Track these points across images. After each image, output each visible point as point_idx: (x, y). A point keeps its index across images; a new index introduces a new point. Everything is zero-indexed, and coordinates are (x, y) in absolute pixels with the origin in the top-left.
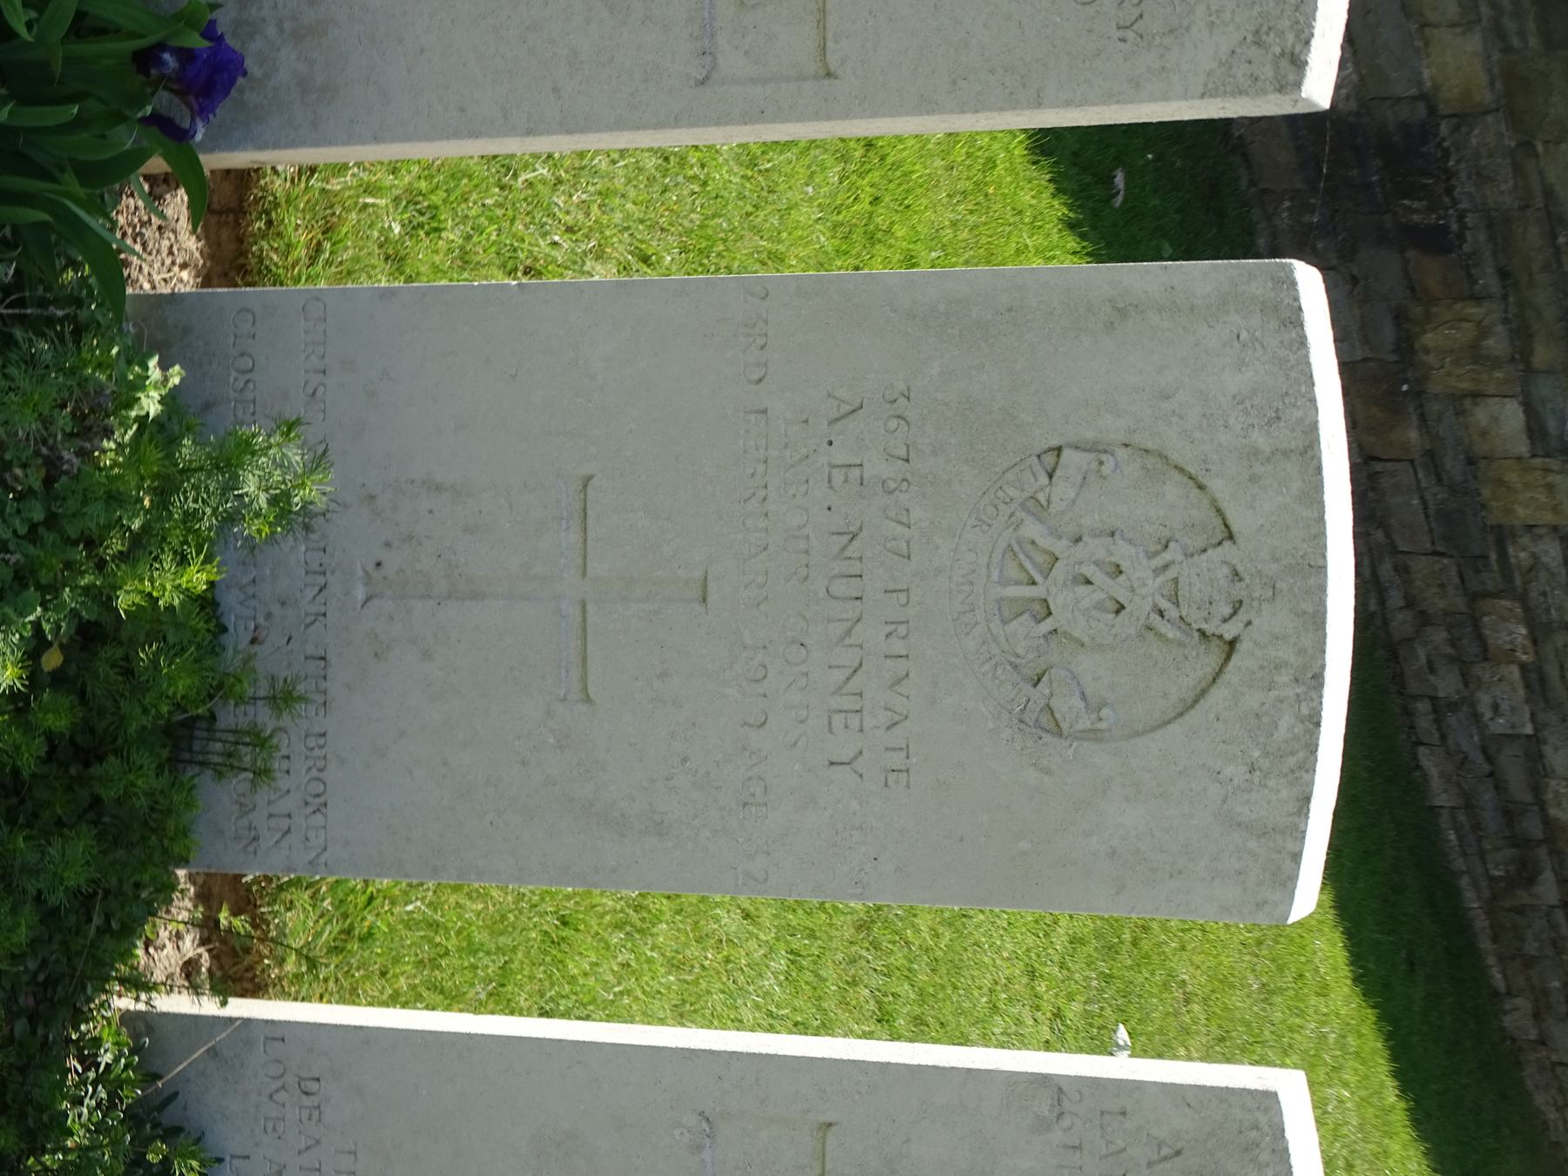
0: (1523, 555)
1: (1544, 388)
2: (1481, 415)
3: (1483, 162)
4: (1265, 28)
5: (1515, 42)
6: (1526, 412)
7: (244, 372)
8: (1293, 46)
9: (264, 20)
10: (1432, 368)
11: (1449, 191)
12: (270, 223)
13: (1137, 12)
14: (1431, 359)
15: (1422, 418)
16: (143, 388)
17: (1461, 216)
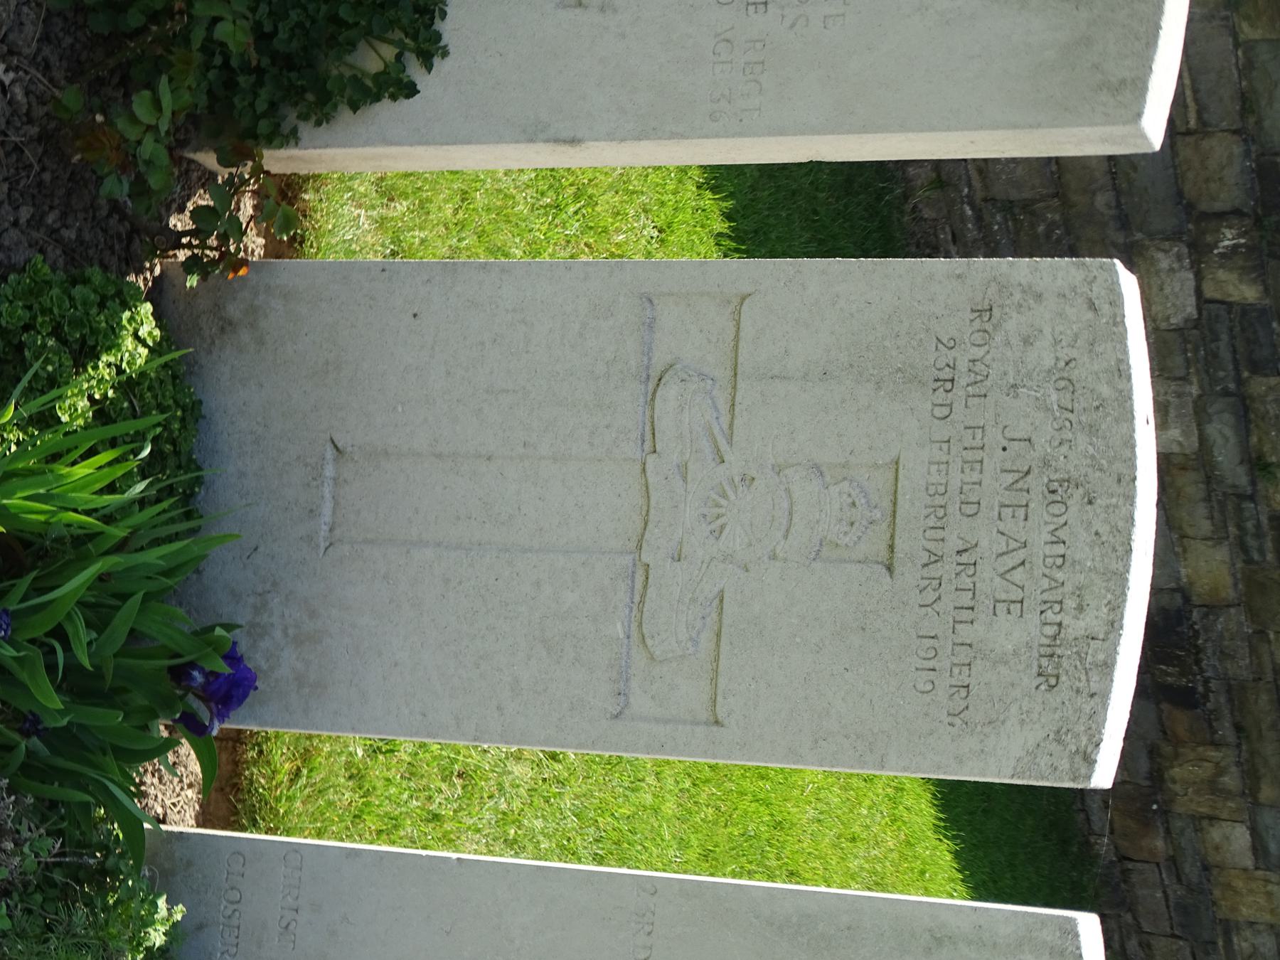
0: (1244, 945)
1: (1267, 818)
2: (1215, 834)
3: (1226, 643)
4: (1064, 730)
5: (1256, 556)
6: (1251, 835)
7: (232, 903)
8: (1086, 747)
9: (272, 625)
10: (1177, 794)
11: (1198, 662)
12: (261, 752)
13: (963, 704)
14: (1177, 788)
15: (1168, 831)
16: (153, 923)
17: (1206, 681)
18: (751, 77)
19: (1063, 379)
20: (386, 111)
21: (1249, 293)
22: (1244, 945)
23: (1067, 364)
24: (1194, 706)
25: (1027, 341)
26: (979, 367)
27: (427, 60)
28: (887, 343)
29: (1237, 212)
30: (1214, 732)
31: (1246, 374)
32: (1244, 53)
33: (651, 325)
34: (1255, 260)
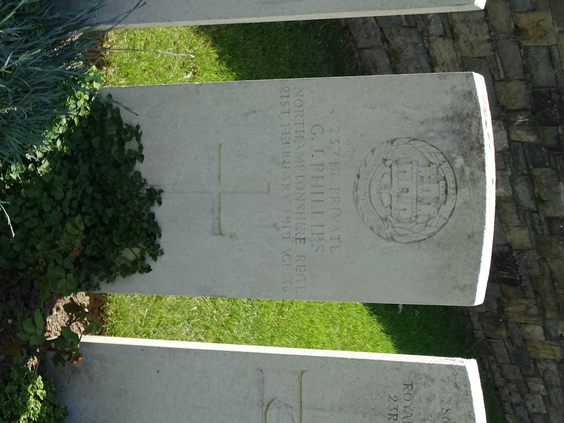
0: (542, 367)
2: (528, 329)
5: (540, 232)
15: (507, 328)
17: (521, 277)
18: (300, 272)
19: (445, 417)
20: (137, 277)
21: (532, 138)
22: (542, 367)
23: (447, 411)
24: (516, 285)
25: (428, 400)
26: (408, 410)
27: (154, 257)
28: (367, 397)
29: (524, 109)
30: (525, 294)
31: (531, 167)
32: (524, 51)
33: (263, 382)
34: (532, 127)
